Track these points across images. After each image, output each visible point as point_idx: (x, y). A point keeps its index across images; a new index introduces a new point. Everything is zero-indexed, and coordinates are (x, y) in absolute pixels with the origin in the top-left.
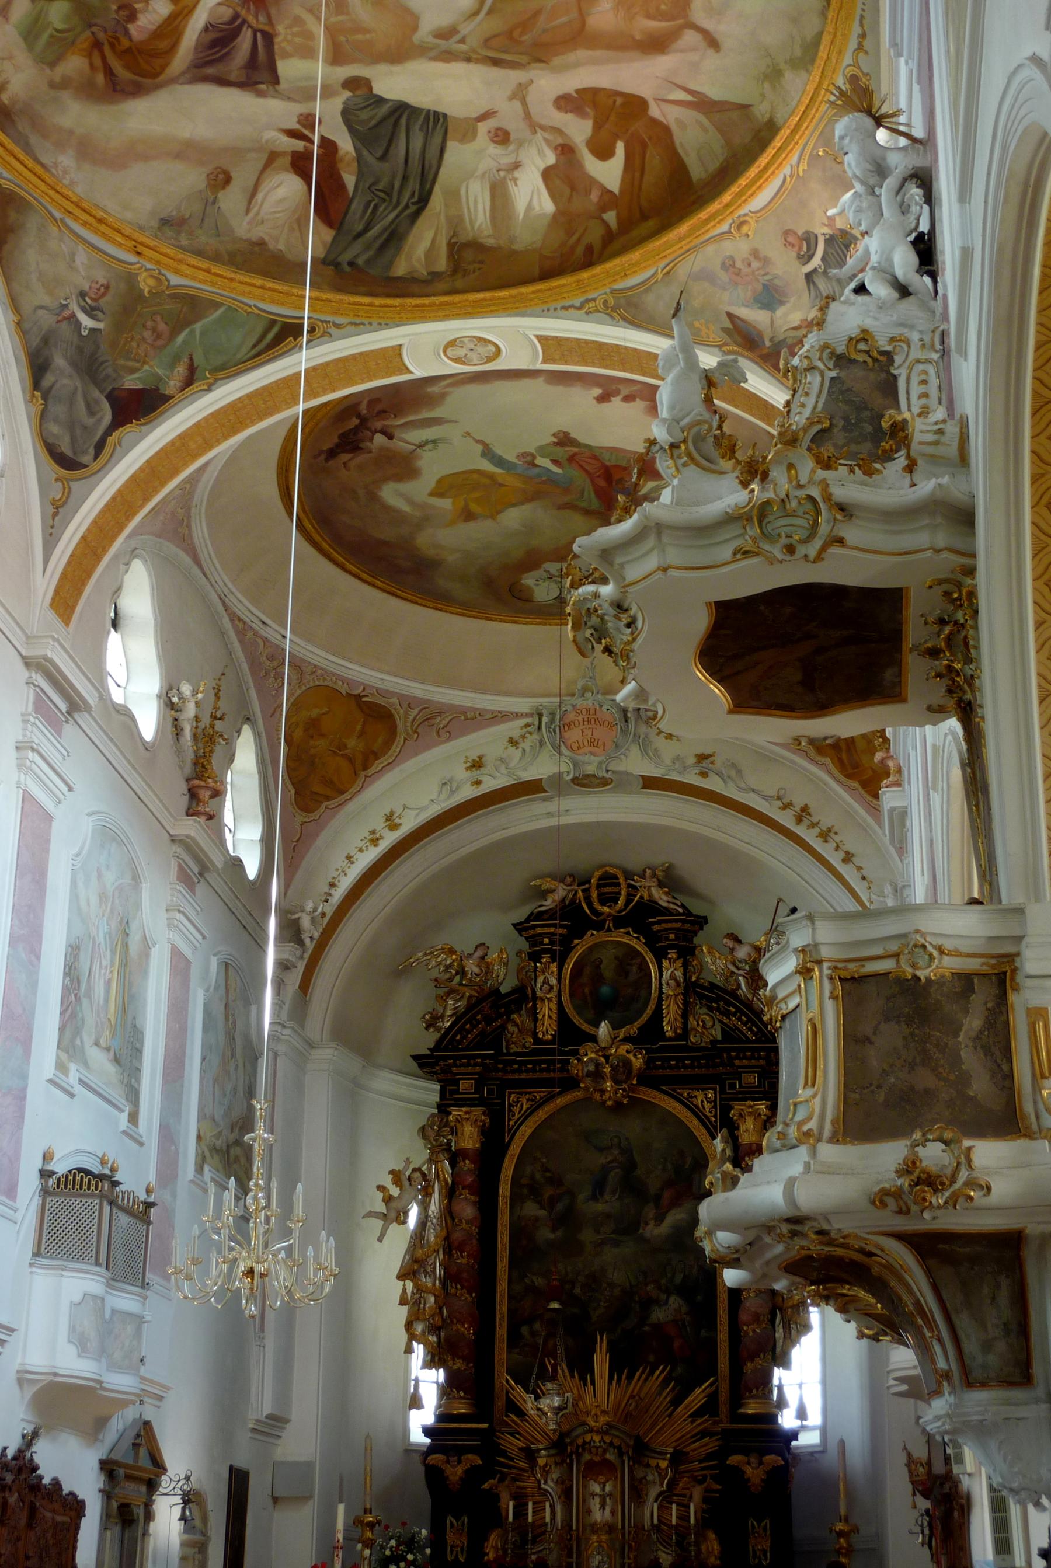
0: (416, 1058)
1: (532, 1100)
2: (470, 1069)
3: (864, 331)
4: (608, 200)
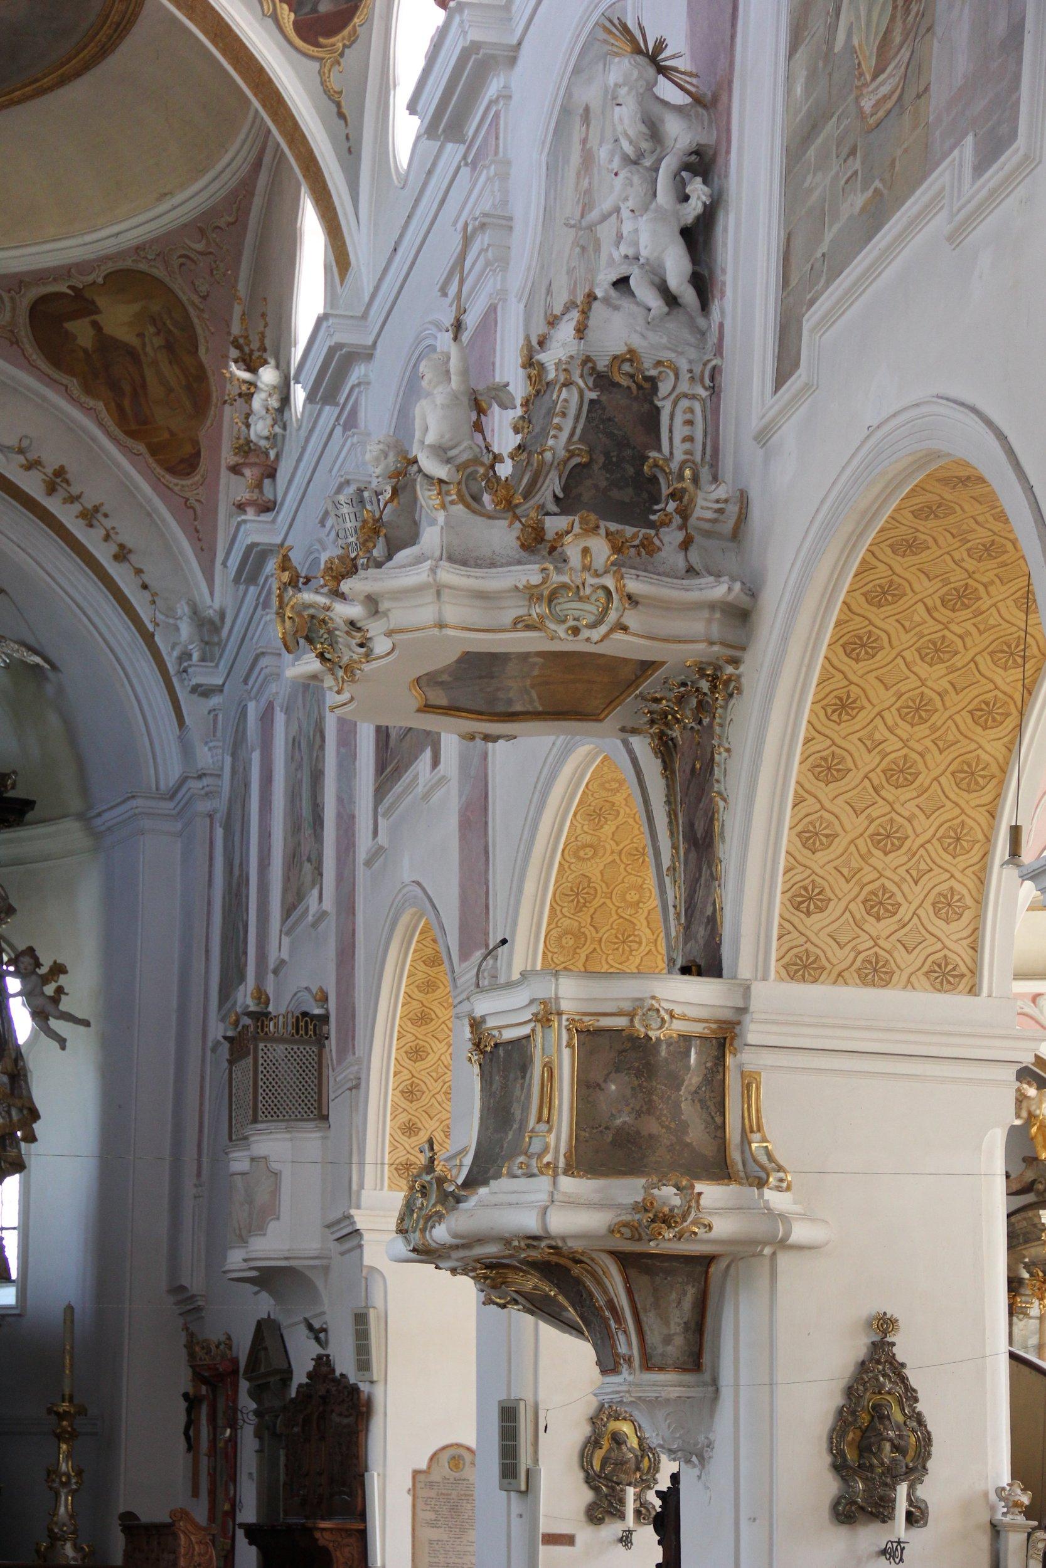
3: (631, 351)
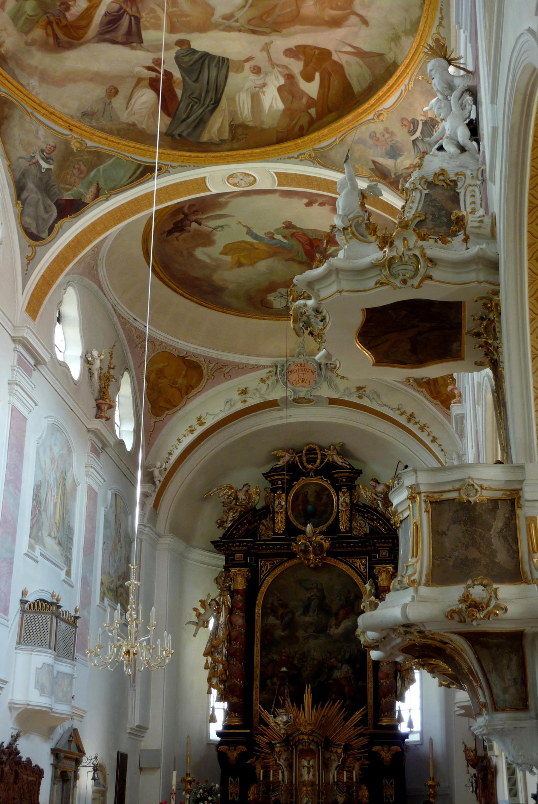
0: (213, 542)
1: (272, 564)
2: (240, 548)
3: (443, 170)
4: (311, 103)
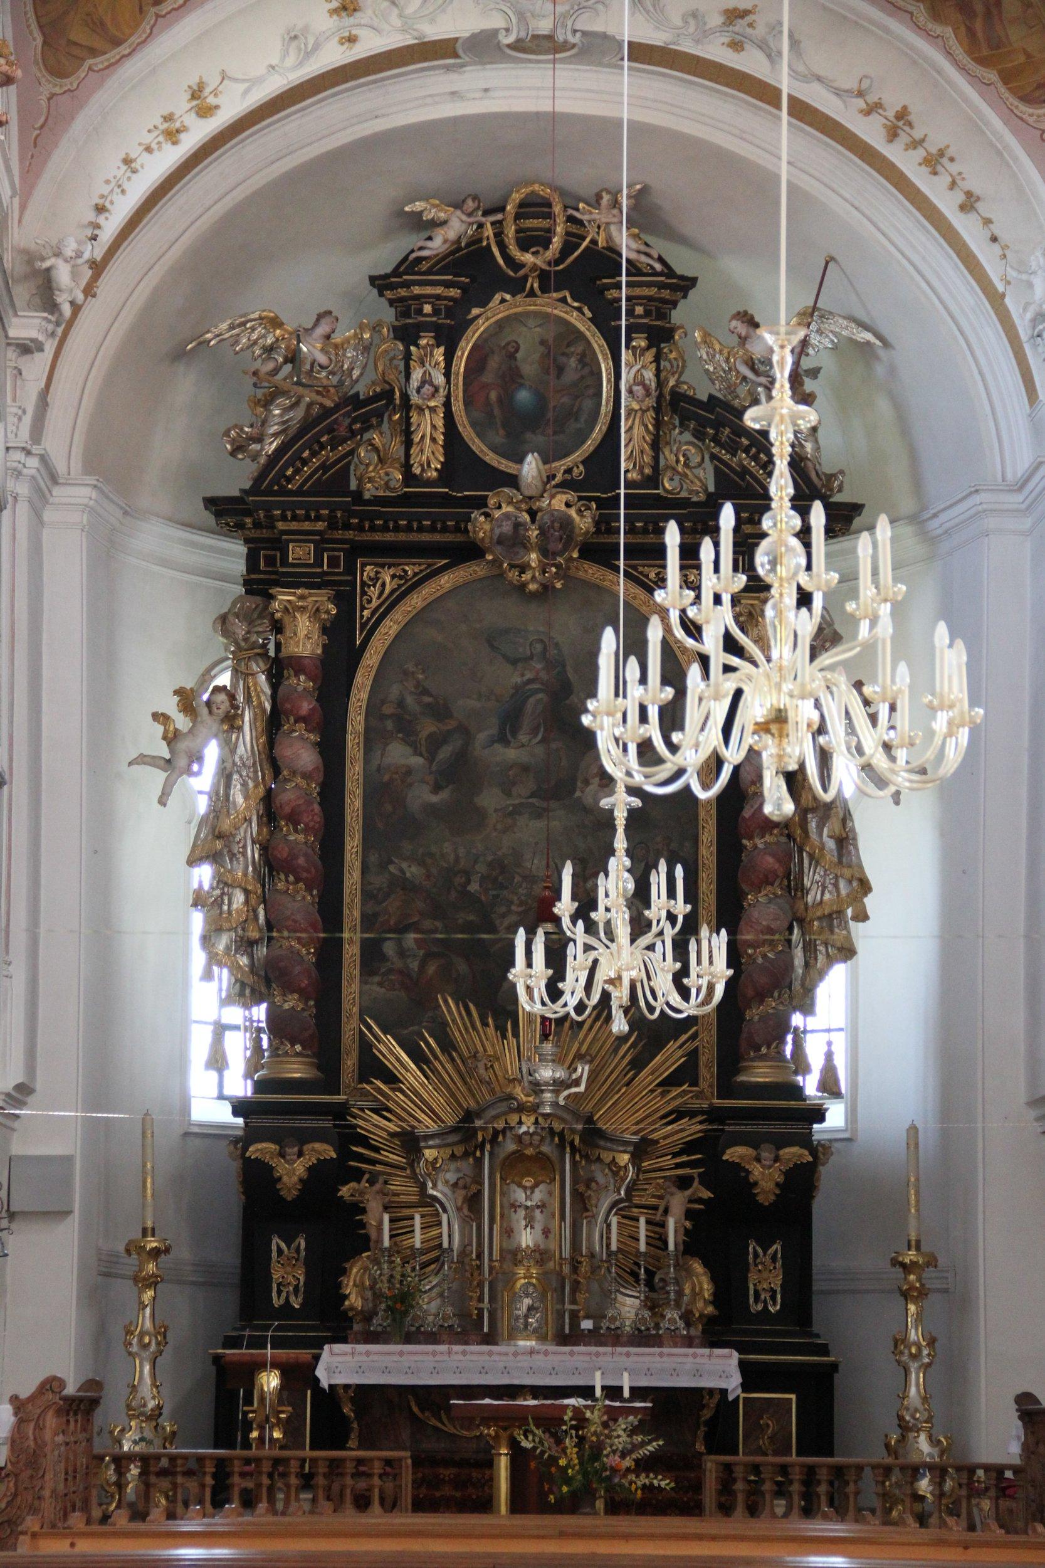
0: (211, 503)
1: (401, 578)
2: (307, 526)
